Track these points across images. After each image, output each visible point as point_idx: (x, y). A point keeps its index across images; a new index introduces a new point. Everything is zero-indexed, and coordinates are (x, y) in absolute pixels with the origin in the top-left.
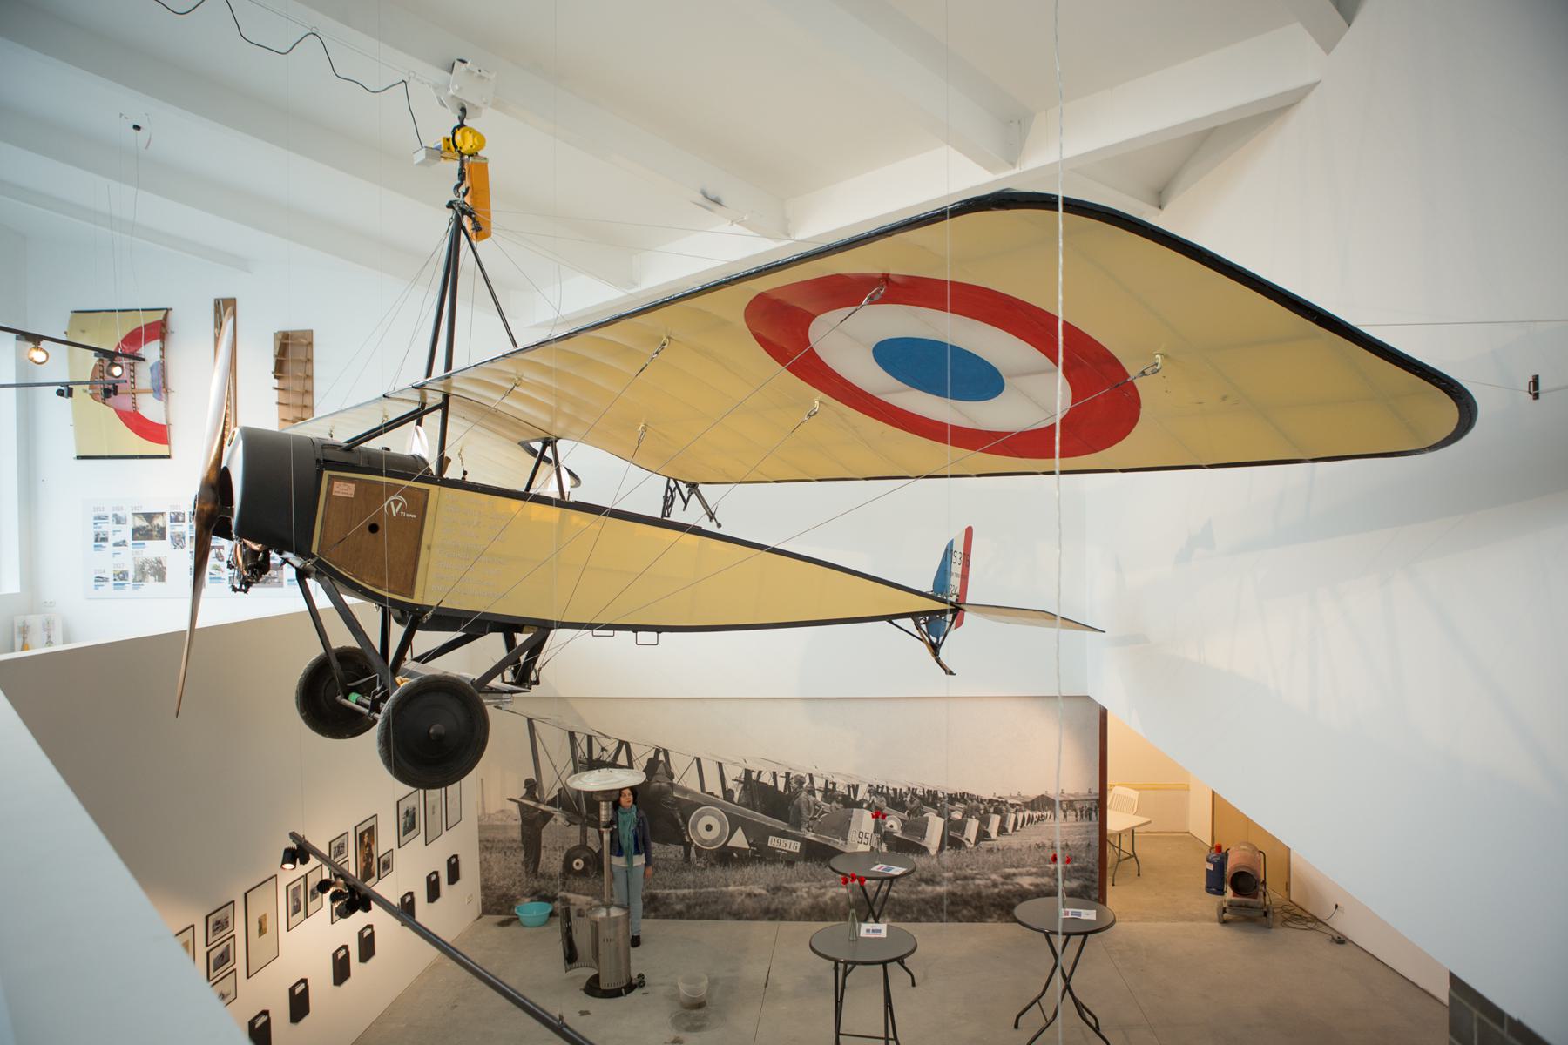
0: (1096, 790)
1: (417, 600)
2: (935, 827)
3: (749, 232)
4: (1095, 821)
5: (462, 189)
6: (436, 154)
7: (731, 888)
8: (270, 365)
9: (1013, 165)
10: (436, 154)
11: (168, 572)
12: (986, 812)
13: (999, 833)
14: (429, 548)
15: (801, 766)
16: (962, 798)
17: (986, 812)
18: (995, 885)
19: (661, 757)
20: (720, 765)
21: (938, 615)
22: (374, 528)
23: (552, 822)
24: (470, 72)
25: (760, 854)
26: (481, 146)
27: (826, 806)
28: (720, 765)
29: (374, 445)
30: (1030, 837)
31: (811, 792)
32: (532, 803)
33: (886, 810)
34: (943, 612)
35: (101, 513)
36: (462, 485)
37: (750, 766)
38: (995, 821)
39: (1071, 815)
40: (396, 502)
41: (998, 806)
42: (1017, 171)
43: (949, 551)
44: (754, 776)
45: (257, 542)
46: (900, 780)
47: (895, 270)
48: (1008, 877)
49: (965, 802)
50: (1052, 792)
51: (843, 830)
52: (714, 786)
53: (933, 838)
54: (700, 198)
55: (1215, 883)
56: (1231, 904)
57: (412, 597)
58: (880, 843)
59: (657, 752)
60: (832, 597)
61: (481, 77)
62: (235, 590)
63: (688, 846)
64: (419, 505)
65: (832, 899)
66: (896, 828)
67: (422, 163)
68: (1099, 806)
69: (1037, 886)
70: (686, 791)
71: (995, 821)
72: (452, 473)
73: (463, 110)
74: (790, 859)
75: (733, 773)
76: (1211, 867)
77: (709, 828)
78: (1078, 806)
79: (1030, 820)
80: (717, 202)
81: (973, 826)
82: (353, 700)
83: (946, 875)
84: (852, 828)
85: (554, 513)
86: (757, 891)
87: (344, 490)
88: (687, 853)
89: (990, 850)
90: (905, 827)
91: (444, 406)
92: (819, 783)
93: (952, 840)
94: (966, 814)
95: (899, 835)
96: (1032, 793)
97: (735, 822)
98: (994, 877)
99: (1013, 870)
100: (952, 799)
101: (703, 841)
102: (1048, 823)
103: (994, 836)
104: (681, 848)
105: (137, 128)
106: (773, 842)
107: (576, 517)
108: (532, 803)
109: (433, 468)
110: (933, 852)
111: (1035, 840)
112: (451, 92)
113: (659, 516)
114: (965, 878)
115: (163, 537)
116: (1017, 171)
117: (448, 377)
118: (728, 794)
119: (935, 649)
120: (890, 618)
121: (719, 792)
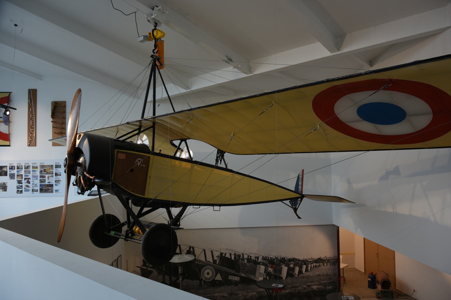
0: (337, 256)
1: (146, 196)
2: (285, 269)
3: (239, 71)
4: (337, 266)
5: (155, 51)
6: (147, 38)
7: (216, 295)
8: (50, 113)
9: (339, 50)
10: (147, 38)
11: (8, 188)
12: (301, 264)
13: (306, 271)
14: (150, 177)
15: (240, 250)
16: (294, 260)
17: (301, 264)
18: (305, 289)
19: (192, 250)
20: (212, 252)
21: (296, 199)
22: (132, 170)
23: (152, 274)
24: (159, 10)
25: (226, 282)
26: (163, 37)
27: (248, 264)
28: (212, 252)
29: (128, 140)
30: (317, 272)
31: (243, 259)
32: (145, 268)
33: (268, 265)
34: (297, 198)
35: (35, 165)
36: (160, 155)
37: (222, 251)
38: (304, 267)
39: (329, 265)
40: (139, 161)
41: (305, 262)
42: (340, 52)
43: (298, 178)
44: (224, 255)
45: (92, 176)
46: (273, 255)
47: (394, 78)
48: (309, 286)
49: (294, 261)
50: (323, 257)
51: (254, 272)
52: (210, 259)
53: (284, 273)
54: (225, 58)
55: (372, 284)
56: (381, 291)
57: (144, 195)
58: (267, 275)
59: (190, 248)
60: (261, 192)
61: (163, 12)
62: (79, 193)
63: (201, 280)
64: (147, 162)
65: (251, 296)
66: (271, 271)
67: (142, 41)
68: (337, 261)
69: (318, 288)
70: (200, 261)
71: (304, 267)
72: (157, 151)
73: (156, 24)
74: (236, 283)
75: (216, 254)
76: (370, 280)
77: (208, 274)
78: (331, 261)
79: (316, 266)
80: (231, 60)
81: (297, 269)
82: (112, 233)
83: (289, 286)
84: (257, 271)
85: (189, 165)
86: (225, 295)
87: (122, 156)
88: (201, 283)
89: (303, 277)
90: (275, 271)
91: (153, 127)
92: (246, 256)
93: (290, 274)
94: (295, 265)
95: (273, 273)
96: (316, 257)
97: (217, 271)
98: (304, 286)
99: (310, 284)
100: (290, 260)
101: (206, 278)
102: (322, 267)
103: (304, 272)
104: (199, 281)
105: (16, 25)
106: (230, 278)
107: (196, 167)
108: (145, 268)
109: (150, 148)
110: (284, 279)
111: (318, 273)
112: (153, 16)
113: (215, 165)
114: (295, 287)
115: (6, 175)
116: (340, 52)
117: (154, 118)
118: (215, 261)
119: (295, 210)
120: (281, 200)
121: (211, 261)
